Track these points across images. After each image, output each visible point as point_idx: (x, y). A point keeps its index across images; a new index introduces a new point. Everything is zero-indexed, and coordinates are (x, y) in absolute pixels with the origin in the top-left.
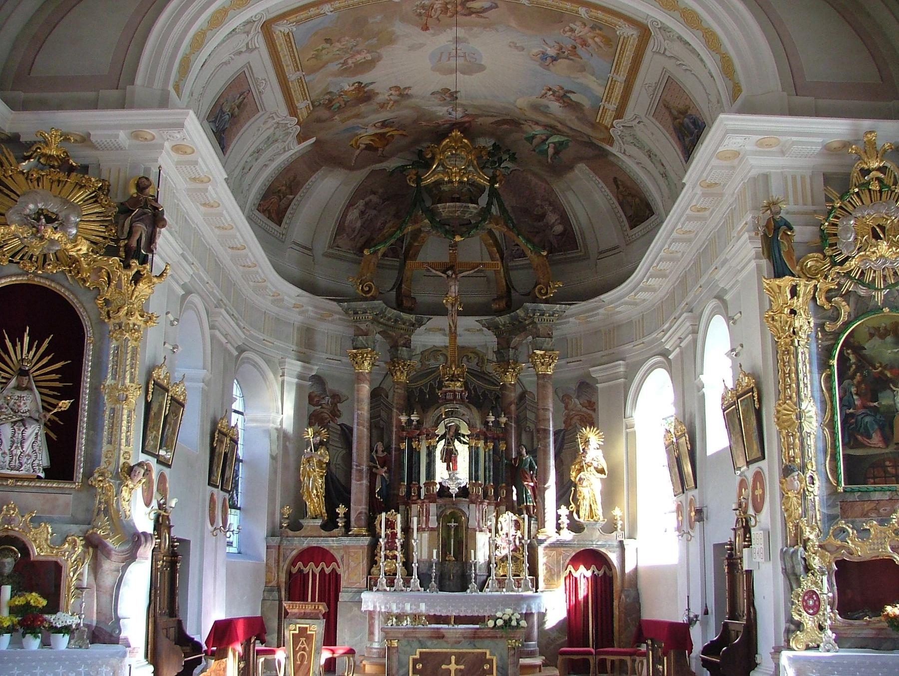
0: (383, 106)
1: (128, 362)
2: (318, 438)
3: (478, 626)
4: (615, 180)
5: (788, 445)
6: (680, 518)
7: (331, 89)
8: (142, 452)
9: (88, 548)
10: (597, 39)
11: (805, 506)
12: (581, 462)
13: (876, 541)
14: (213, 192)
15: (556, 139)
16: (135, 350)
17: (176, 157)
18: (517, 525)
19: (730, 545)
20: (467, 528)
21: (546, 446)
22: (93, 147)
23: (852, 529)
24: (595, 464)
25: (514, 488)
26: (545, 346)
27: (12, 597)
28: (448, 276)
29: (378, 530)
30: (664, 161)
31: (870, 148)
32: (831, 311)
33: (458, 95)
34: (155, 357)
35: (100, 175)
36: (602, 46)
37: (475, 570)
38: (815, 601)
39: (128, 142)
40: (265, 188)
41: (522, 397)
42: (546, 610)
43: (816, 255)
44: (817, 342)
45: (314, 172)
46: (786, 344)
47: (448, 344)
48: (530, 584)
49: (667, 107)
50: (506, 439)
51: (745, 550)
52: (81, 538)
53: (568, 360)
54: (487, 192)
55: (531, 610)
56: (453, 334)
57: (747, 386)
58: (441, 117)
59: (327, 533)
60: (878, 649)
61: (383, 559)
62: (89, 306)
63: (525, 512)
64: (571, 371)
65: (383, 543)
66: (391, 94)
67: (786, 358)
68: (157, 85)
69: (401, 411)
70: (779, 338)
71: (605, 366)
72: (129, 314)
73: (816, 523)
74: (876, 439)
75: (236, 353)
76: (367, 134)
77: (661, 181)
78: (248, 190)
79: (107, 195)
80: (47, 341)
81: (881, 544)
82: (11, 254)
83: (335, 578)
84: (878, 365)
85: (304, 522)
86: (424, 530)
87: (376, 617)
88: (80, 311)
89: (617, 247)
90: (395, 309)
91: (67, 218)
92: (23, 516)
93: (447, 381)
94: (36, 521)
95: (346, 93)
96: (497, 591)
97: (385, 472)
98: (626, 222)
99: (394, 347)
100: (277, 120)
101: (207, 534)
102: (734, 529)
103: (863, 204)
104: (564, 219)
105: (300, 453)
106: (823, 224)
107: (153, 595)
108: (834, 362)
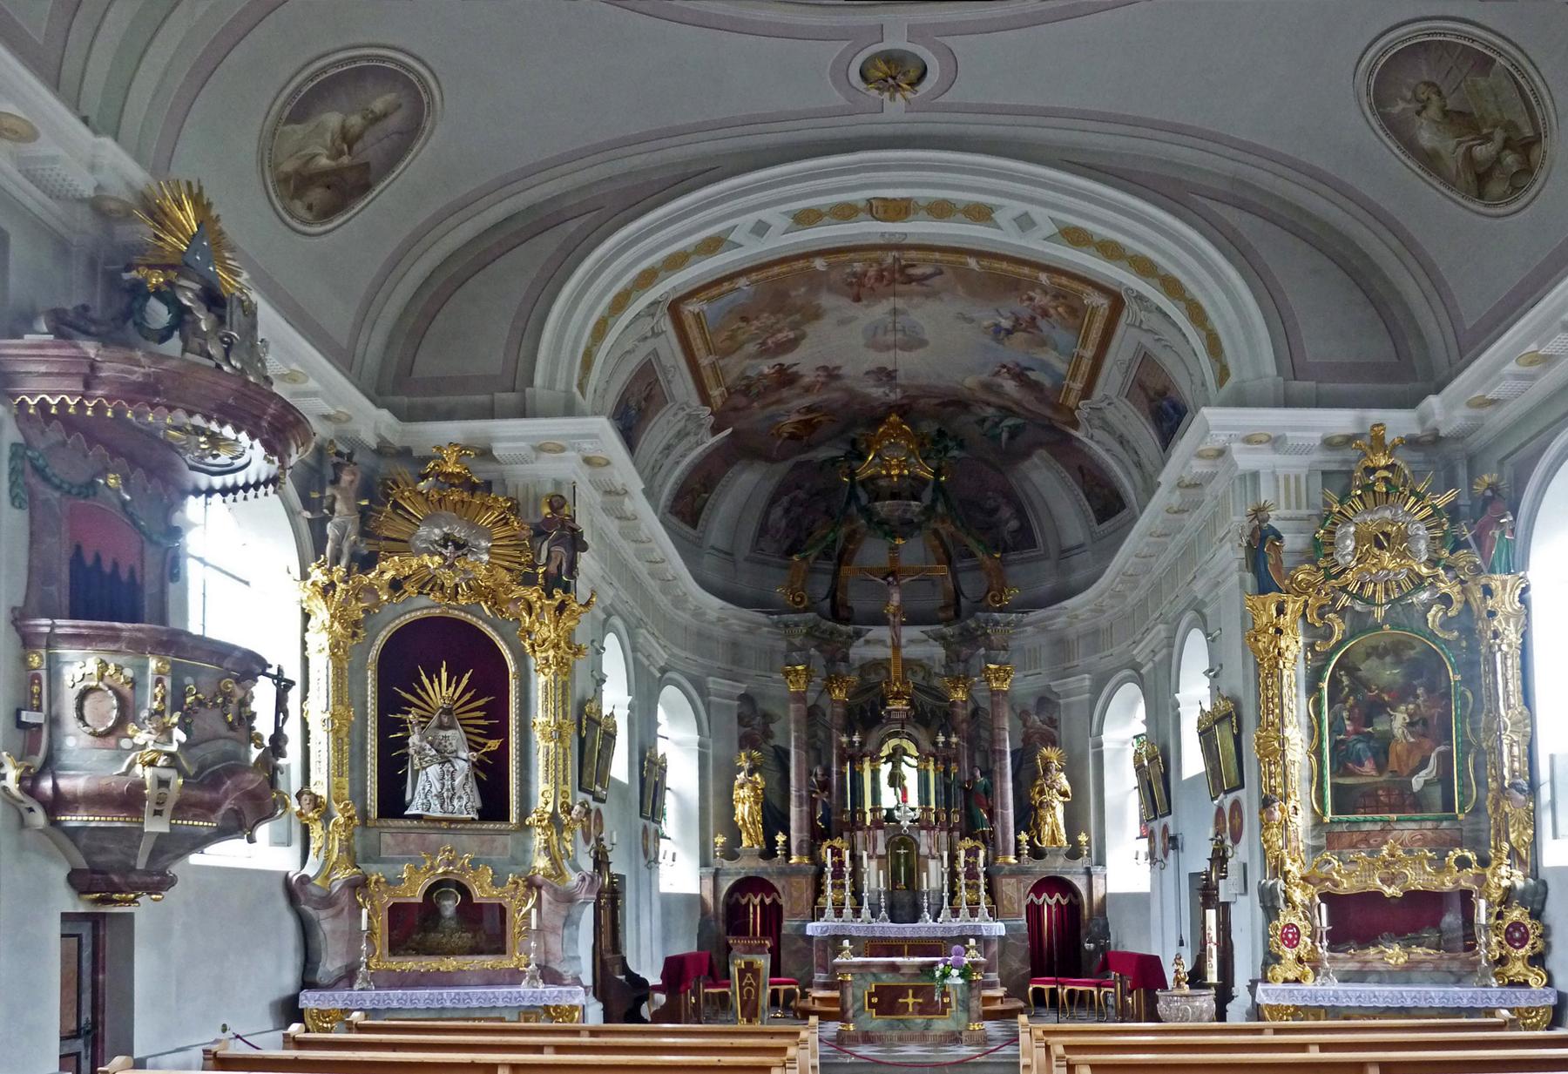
0: (808, 390)
4: (1080, 469)
7: (748, 373)
15: (1010, 422)
20: (918, 854)
21: (1003, 768)
22: (494, 459)
26: (1000, 659)
30: (1137, 447)
41: (976, 712)
43: (1307, 566)
46: (1270, 666)
49: (1142, 386)
50: (957, 760)
51: (1221, 882)
56: (896, 647)
58: (877, 399)
61: (829, 889)
67: (1269, 682)
68: (560, 386)
74: (1368, 767)
75: (658, 675)
80: (467, 676)
95: (765, 376)
98: (1092, 516)
99: (831, 662)
100: (688, 410)
108: (1325, 685)
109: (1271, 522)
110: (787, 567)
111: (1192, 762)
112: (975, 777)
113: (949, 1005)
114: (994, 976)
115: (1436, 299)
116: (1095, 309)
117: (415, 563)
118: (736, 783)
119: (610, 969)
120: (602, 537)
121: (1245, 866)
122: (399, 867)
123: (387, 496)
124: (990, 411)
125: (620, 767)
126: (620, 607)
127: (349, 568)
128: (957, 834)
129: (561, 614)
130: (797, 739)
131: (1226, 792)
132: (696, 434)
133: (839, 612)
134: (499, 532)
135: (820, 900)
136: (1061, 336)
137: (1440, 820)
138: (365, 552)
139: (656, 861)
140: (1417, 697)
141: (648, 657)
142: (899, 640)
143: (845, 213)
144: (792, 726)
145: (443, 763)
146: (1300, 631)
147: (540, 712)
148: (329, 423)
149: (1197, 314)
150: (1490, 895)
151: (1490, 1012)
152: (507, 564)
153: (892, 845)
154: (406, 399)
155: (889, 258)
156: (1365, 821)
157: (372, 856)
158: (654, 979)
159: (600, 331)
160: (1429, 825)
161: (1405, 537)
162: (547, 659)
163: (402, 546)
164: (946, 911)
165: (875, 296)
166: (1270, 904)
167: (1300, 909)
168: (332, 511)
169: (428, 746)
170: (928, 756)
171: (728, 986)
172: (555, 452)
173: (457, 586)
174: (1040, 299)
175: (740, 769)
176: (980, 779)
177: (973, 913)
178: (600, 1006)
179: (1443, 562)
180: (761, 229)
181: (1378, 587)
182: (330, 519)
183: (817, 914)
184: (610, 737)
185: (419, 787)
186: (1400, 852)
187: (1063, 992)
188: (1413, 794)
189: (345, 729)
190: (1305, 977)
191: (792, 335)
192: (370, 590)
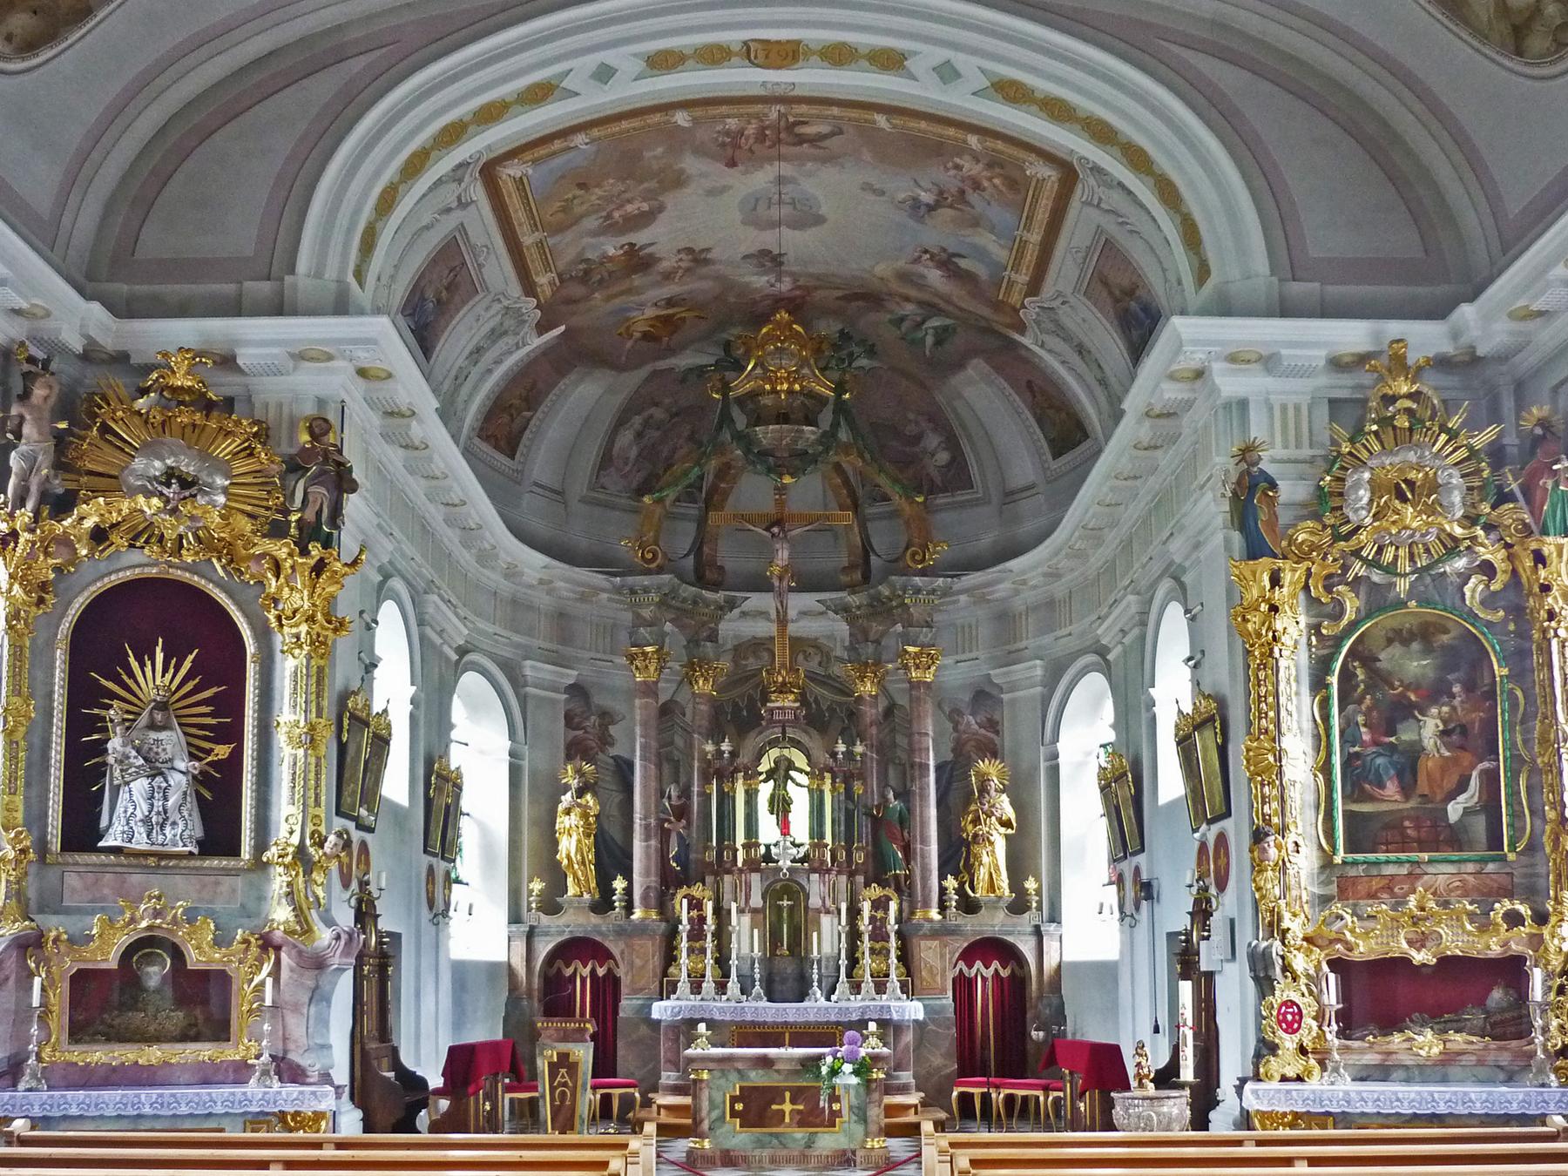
0: (668, 276)
4: (1029, 384)
8: (337, 814)
10: (996, 181)
15: (935, 322)
19: (1185, 934)
20: (807, 907)
23: (1352, 916)
28: (773, 535)
33: (784, 259)
36: (1004, 189)
40: (489, 403)
41: (889, 712)
43: (1310, 523)
45: (563, 376)
46: (1262, 654)
49: (1105, 283)
50: (862, 776)
51: (1203, 943)
53: (959, 657)
54: (830, 407)
56: (782, 621)
61: (684, 954)
66: (681, 260)
67: (1262, 675)
68: (331, 273)
70: (1252, 646)
73: (1302, 907)
74: (1392, 789)
75: (455, 657)
76: (645, 315)
80: (191, 658)
81: (1392, 936)
95: (611, 259)
97: (684, 828)
100: (506, 303)
108: (1334, 680)
109: (1262, 465)
110: (636, 511)
111: (1170, 783)
112: (887, 801)
113: (838, 1114)
114: (906, 1077)
115: (1469, 176)
116: (1041, 182)
117: (125, 506)
118: (561, 808)
119: (375, 1063)
120: (379, 470)
121: (1232, 922)
122: (87, 919)
124: (910, 308)
125: (397, 783)
126: (402, 564)
127: (37, 513)
128: (860, 879)
129: (318, 576)
130: (644, 748)
131: (1210, 822)
133: (706, 574)
134: (240, 466)
135: (672, 970)
136: (998, 214)
137: (1483, 861)
138: (60, 491)
139: (445, 913)
140: (1453, 696)
141: (441, 633)
142: (785, 612)
143: (714, 56)
144: (638, 730)
145: (153, 777)
146: (1301, 609)
147: (286, 708)
148: (20, 320)
149: (1168, 193)
150: (1548, 963)
151: (1542, 1119)
152: (249, 508)
153: (768, 893)
154: (126, 287)
155: (773, 112)
156: (1387, 862)
157: (52, 903)
158: (435, 1081)
159: (387, 202)
160: (1470, 868)
161: (1433, 486)
162: (298, 637)
163: (110, 484)
164: (843, 986)
165: (756, 161)
166: (1263, 974)
167: (1303, 980)
168: (18, 436)
169: (134, 753)
170: (822, 772)
171: (535, 1089)
172: (318, 360)
173: (181, 537)
174: (970, 167)
175: (567, 788)
176: (894, 804)
177: (880, 988)
178: (359, 1114)
179: (1483, 520)
180: (604, 74)
181: (1401, 552)
182: (15, 447)
183: (667, 989)
184: (381, 743)
185: (120, 809)
186: (1432, 904)
187: (998, 1097)
188: (1450, 825)
189: (22, 729)
190: (1310, 1073)
191: (645, 207)
192: (65, 541)
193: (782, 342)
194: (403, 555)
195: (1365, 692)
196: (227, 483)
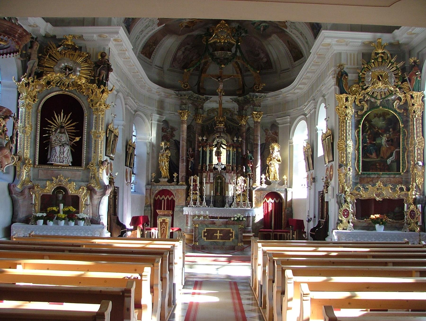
1: (100, 123)
2: (166, 146)
3: (228, 220)
4: (288, 41)
5: (342, 156)
6: (308, 181)
9: (88, 190)
11: (346, 179)
12: (271, 157)
13: (370, 192)
14: (128, 54)
16: (102, 118)
17: (115, 43)
18: (245, 182)
19: (322, 192)
20: (225, 182)
24: (276, 158)
25: (244, 167)
26: (258, 110)
27: (64, 208)
28: (219, 81)
29: (190, 183)
31: (380, 45)
32: (361, 107)
34: (108, 120)
35: (86, 51)
37: (228, 199)
38: (347, 213)
39: (97, 38)
40: (144, 44)
41: (249, 129)
42: (255, 215)
44: (355, 118)
47: (218, 107)
48: (249, 205)
52: (86, 187)
54: (235, 47)
55: (249, 215)
56: (221, 104)
57: (329, 133)
59: (170, 184)
60: (368, 230)
61: (192, 194)
62: (85, 102)
63: (248, 176)
64: (268, 120)
65: (192, 188)
69: (199, 135)
70: (340, 117)
71: (282, 118)
72: (100, 105)
73: (350, 185)
74: (374, 155)
75: (134, 113)
77: (306, 44)
78: (138, 46)
79: (89, 59)
80: (70, 115)
82: (56, 83)
83: (173, 201)
84: (376, 128)
85: (160, 179)
86: (208, 183)
87: (189, 217)
88: (82, 104)
89: (289, 69)
90: (197, 94)
91: (76, 68)
92: (65, 179)
93: (218, 123)
94: (70, 181)
96: (236, 207)
97: (193, 160)
99: (197, 109)
101: (125, 185)
102: (324, 186)
103: (375, 66)
104: (267, 56)
105: (158, 152)
106: (360, 74)
107: (109, 207)
108: (361, 126)
111: (320, 152)
112: (248, 154)
123: (47, 52)
132: (152, 26)
140: (390, 132)
160: (392, 176)
193: (222, 29)
194: (122, 86)
195: (368, 130)
196: (80, 69)
